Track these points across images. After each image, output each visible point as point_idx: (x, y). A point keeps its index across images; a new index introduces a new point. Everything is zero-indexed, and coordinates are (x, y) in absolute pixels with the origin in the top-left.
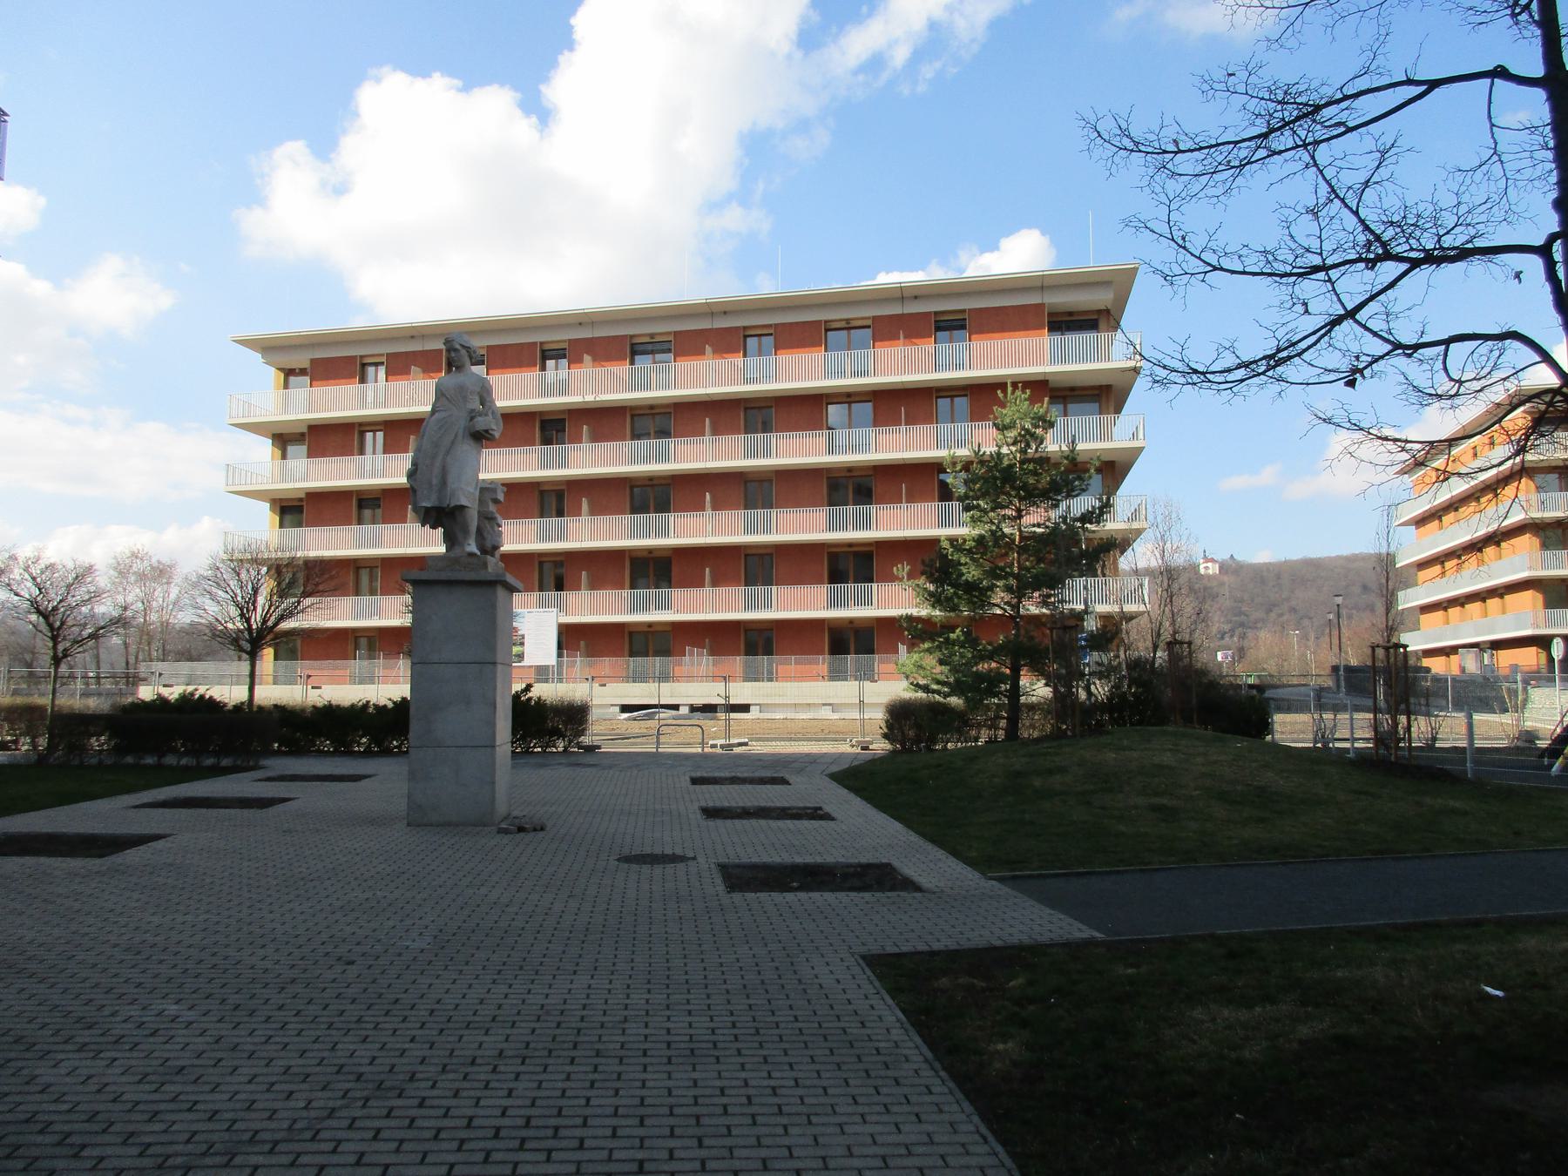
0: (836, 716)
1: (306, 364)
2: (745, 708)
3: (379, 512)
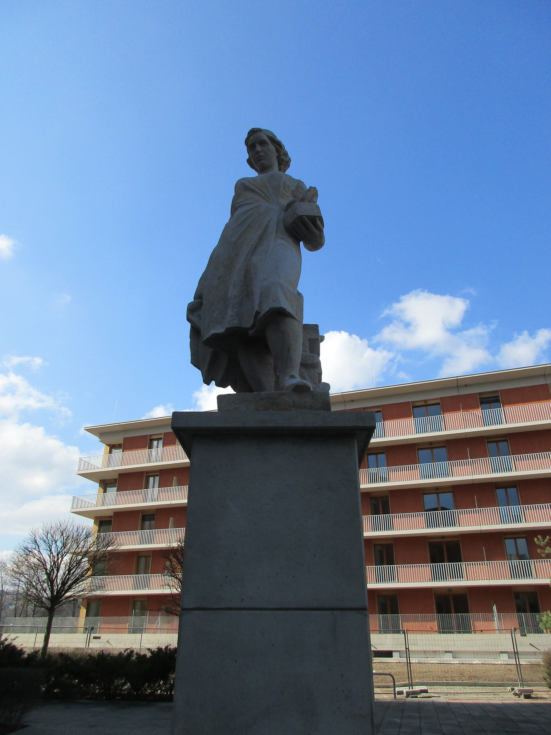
0: (456, 661)
1: (121, 442)
2: (389, 654)
3: (153, 523)
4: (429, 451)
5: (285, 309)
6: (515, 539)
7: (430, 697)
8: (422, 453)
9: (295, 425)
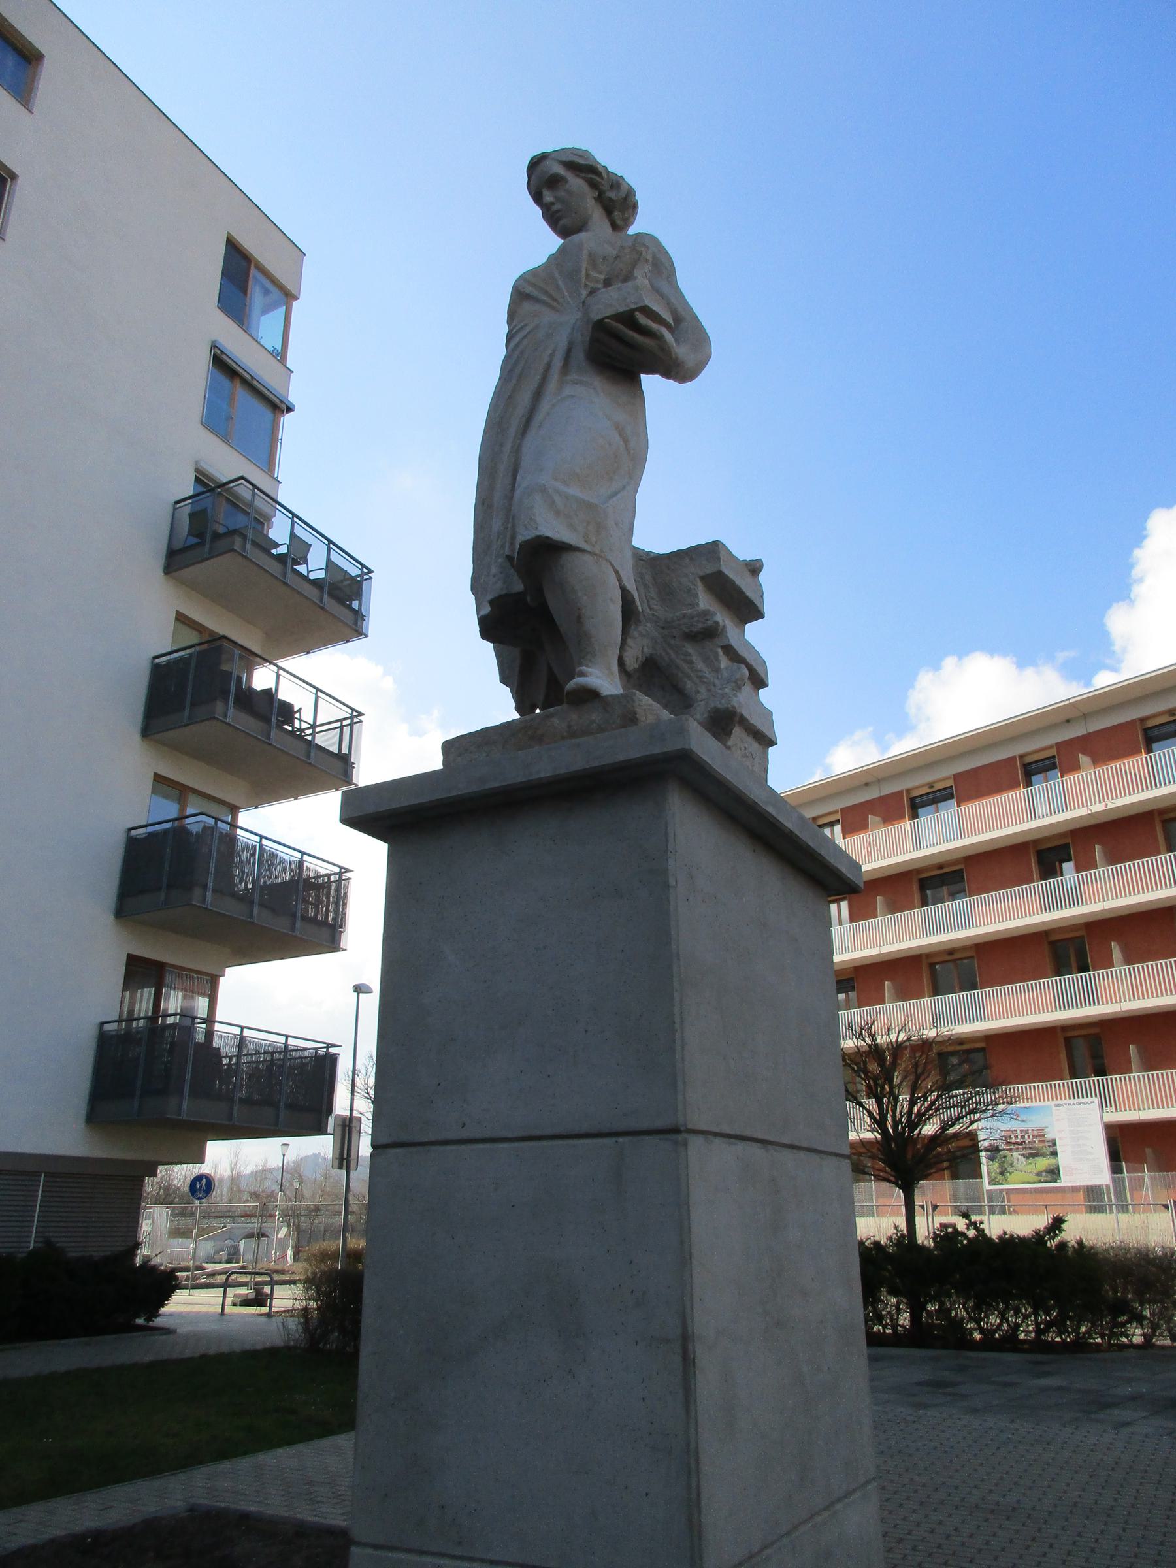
3: (853, 995)
5: (548, 538)
9: (536, 777)
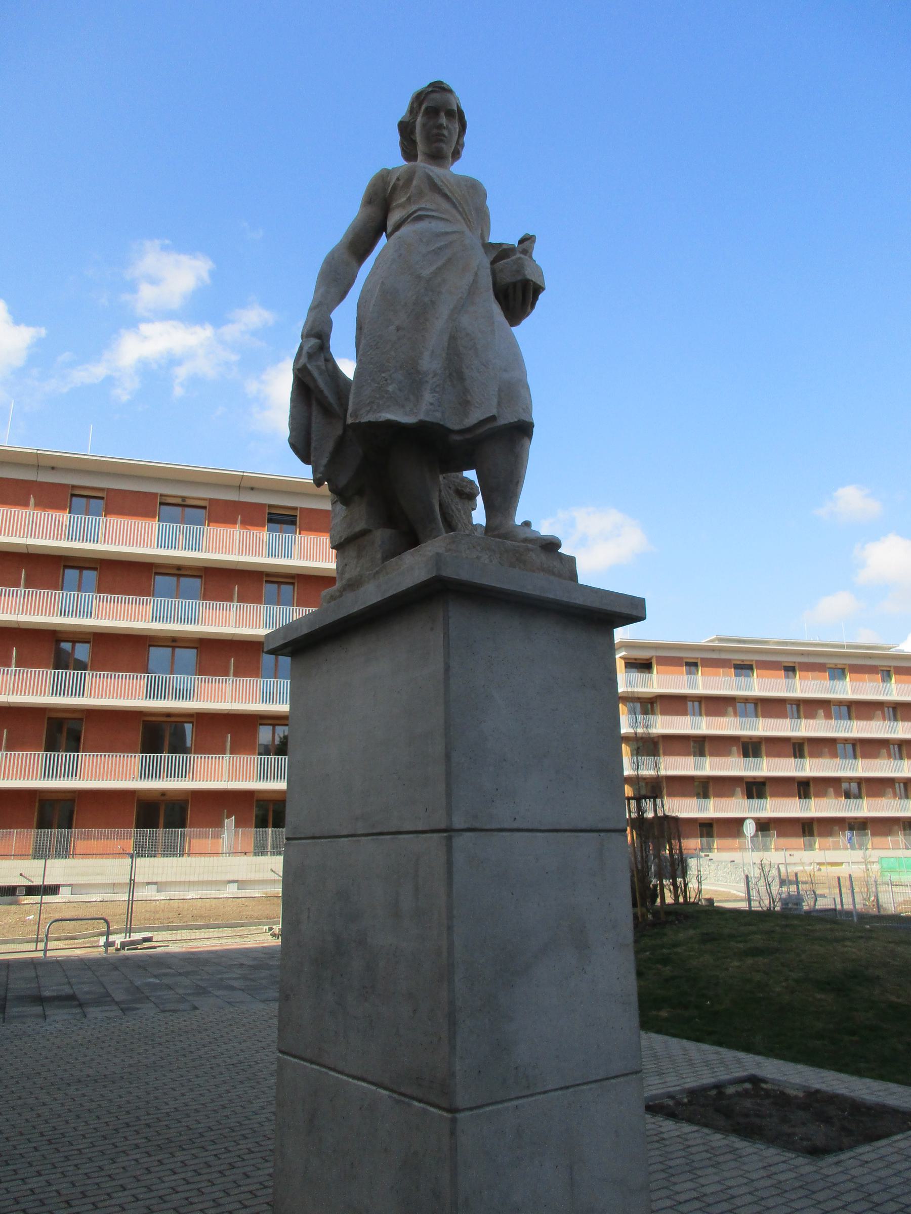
0: (161, 896)
2: (53, 890)
4: (174, 579)
6: (274, 725)
7: (154, 947)
8: (160, 581)
